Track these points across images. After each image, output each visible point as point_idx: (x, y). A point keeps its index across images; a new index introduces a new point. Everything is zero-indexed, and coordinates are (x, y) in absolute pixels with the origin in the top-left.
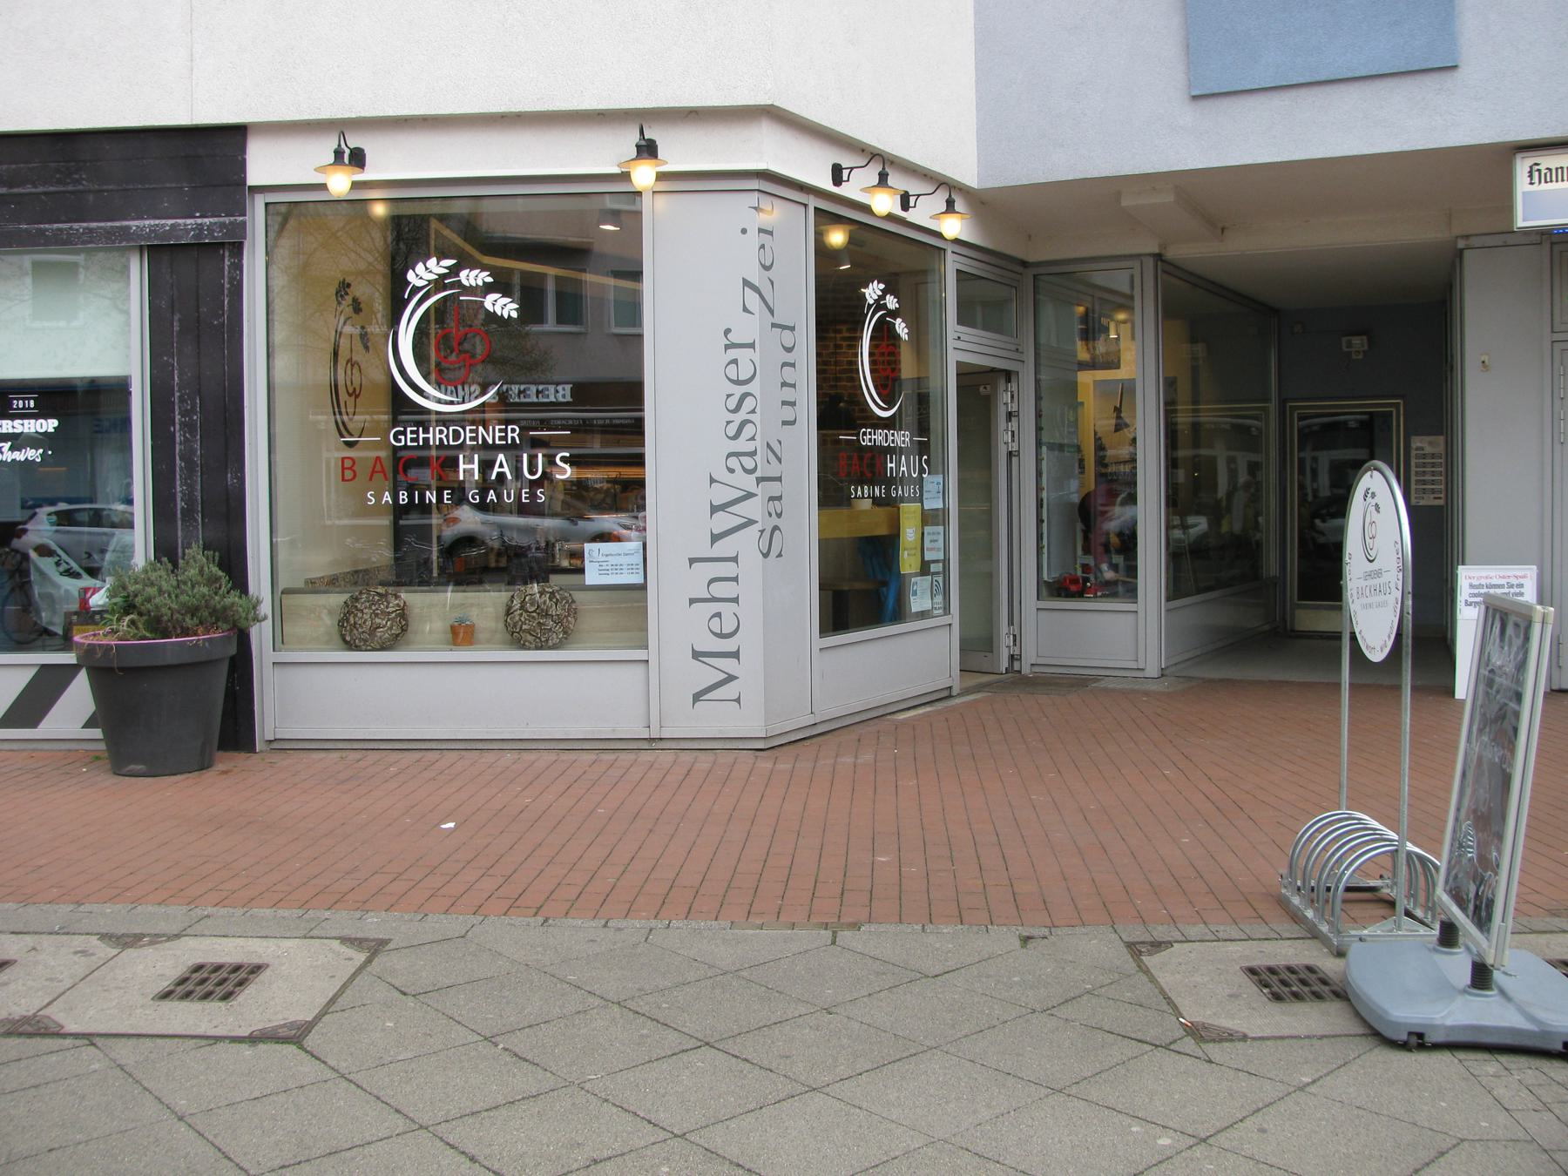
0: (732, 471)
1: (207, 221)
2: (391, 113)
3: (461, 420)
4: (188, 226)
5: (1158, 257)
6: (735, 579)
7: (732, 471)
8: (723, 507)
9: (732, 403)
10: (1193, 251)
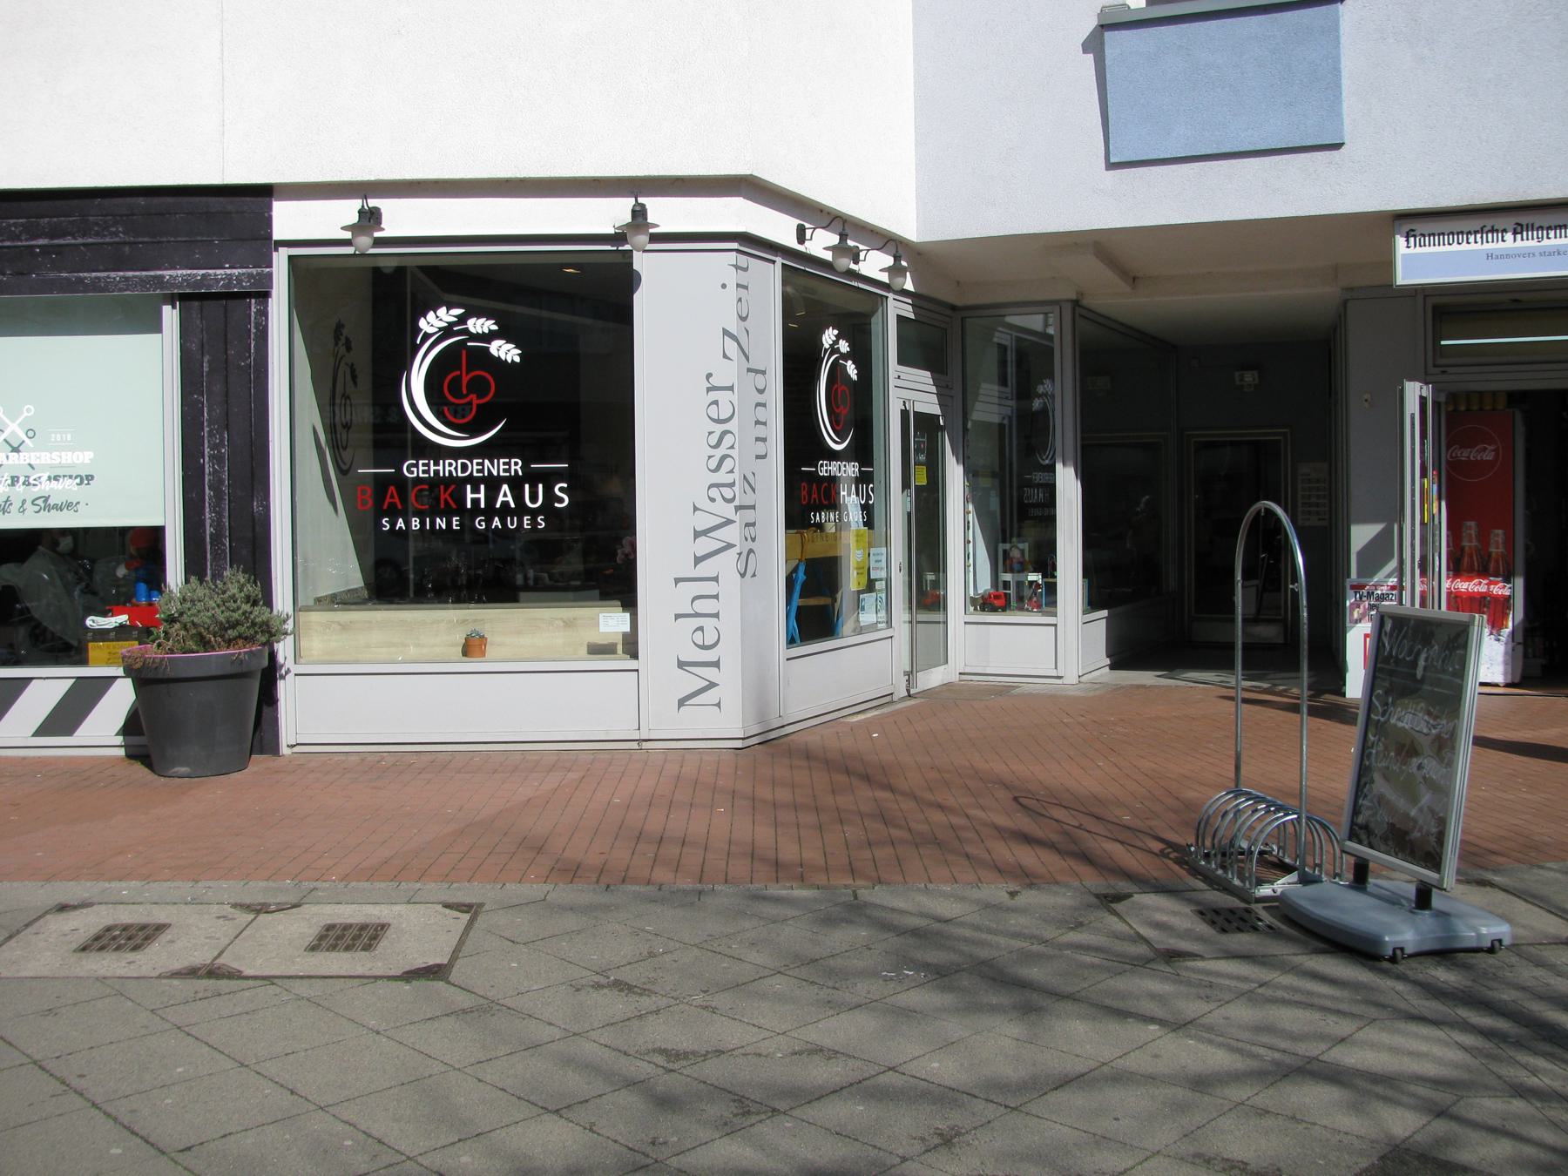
0: (713, 500)
1: (236, 272)
2: (408, 177)
3: (469, 453)
4: (223, 275)
5: (1076, 303)
6: (716, 597)
7: (713, 500)
8: (705, 533)
9: (714, 440)
10: (1112, 298)
